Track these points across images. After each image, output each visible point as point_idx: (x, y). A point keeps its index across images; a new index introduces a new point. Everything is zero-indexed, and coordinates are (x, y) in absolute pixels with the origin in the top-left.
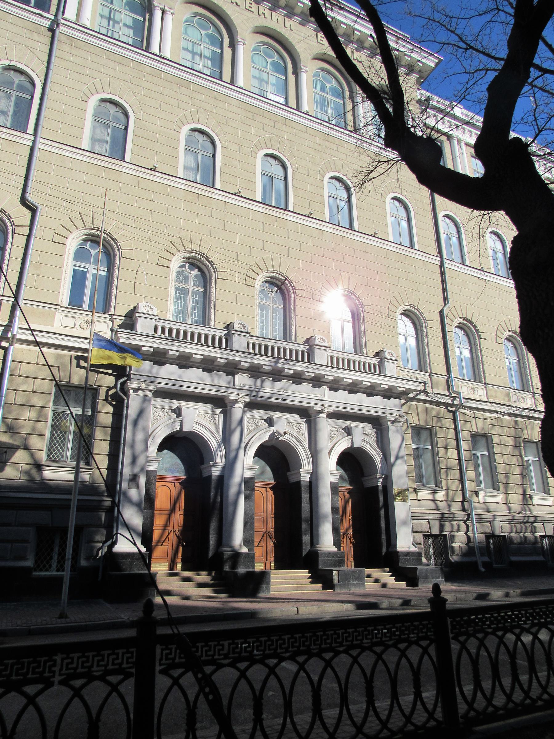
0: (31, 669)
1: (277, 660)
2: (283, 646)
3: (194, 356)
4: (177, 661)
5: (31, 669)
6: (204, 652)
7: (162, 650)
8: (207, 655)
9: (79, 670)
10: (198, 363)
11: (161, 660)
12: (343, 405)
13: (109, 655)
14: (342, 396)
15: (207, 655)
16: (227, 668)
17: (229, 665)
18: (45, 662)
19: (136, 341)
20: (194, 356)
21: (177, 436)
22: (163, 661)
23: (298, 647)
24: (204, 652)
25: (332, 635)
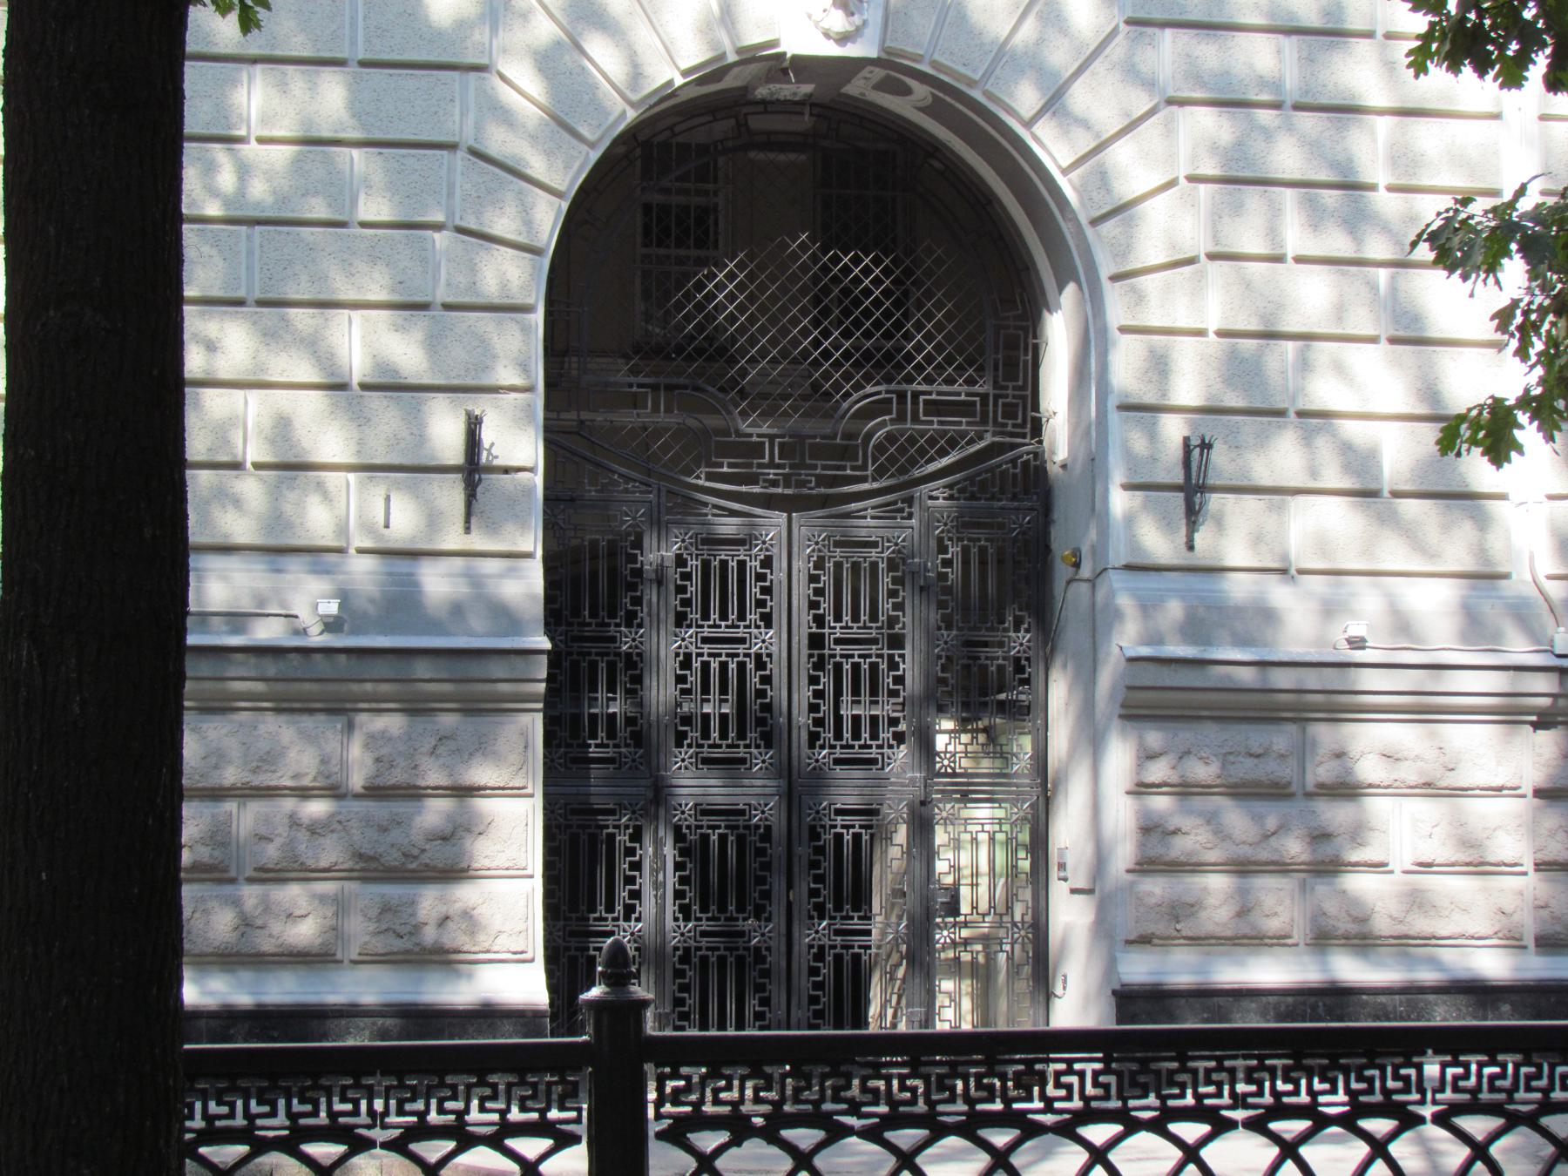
1: (1016, 1132)
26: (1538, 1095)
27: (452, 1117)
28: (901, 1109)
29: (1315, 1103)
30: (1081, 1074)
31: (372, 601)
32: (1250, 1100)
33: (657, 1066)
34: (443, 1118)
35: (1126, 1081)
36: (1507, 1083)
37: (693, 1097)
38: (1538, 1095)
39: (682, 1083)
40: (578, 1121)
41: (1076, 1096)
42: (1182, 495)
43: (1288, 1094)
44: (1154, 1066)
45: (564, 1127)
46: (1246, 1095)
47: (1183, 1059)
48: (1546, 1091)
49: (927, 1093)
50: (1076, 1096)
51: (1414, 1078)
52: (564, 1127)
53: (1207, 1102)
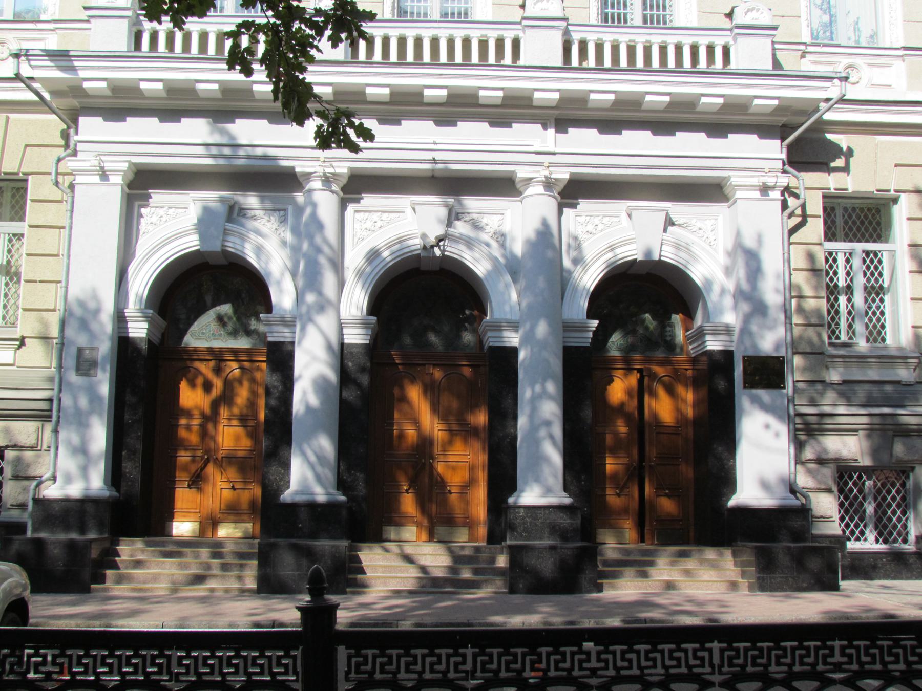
0: (749, 660)
1: (882, 682)
2: (806, 660)
3: (593, 96)
4: (749, 669)
5: (749, 660)
6: (479, 665)
7: (349, 658)
8: (557, 669)
9: (503, 674)
10: (714, 113)
11: (348, 673)
12: (429, 156)
13: (424, 657)
14: (584, 140)
15: (557, 669)
16: (839, 686)
17: (843, 682)
18: (549, 655)
19: (519, 82)
20: (593, 96)
21: (631, 272)
22: (353, 675)
23: (743, 667)
24: (479, 665)
25: (793, 649)
26: (785, 668)
27: (390, 675)
28: (79, 678)
29: (643, 674)
30: (169, 658)
31: (466, 329)
32: (599, 672)
33: (347, 648)
34: (510, 674)
35: (250, 662)
36: (393, 667)
37: (788, 660)
38: (785, 668)
39: (40, 659)
40: (297, 681)
41: (707, 664)
42: (84, 121)
43: (647, 667)
44: (902, 643)
45: (39, 683)
46: (178, 674)
47: (873, 640)
48: (790, 666)
49: (246, 667)
50: (707, 664)
51: (165, 665)
52: (39, 683)
53: (279, 678)
